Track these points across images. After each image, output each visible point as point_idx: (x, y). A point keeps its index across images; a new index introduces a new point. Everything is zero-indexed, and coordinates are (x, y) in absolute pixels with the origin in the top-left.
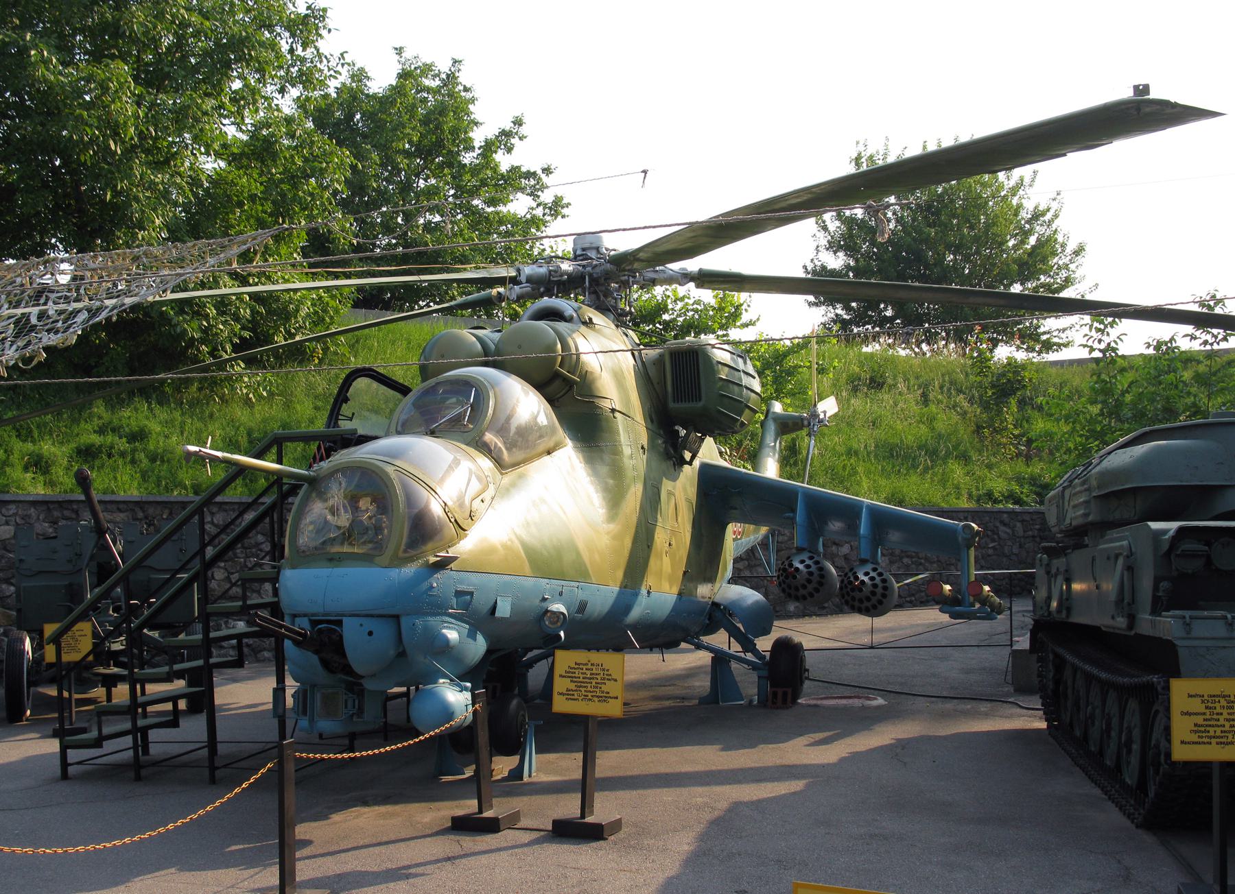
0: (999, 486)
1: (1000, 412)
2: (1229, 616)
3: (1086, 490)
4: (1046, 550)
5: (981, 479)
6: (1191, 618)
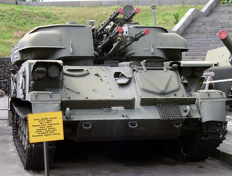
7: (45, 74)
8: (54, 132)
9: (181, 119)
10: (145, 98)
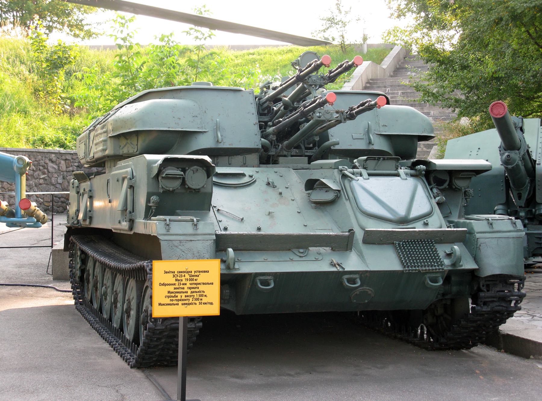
0: (49, 134)
1: (52, 80)
2: (195, 219)
3: (104, 132)
4: (77, 177)
5: (37, 128)
6: (170, 220)
7: (181, 181)
8: (201, 300)
9: (441, 270)
10: (375, 229)
